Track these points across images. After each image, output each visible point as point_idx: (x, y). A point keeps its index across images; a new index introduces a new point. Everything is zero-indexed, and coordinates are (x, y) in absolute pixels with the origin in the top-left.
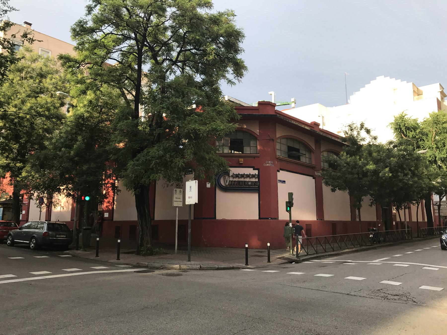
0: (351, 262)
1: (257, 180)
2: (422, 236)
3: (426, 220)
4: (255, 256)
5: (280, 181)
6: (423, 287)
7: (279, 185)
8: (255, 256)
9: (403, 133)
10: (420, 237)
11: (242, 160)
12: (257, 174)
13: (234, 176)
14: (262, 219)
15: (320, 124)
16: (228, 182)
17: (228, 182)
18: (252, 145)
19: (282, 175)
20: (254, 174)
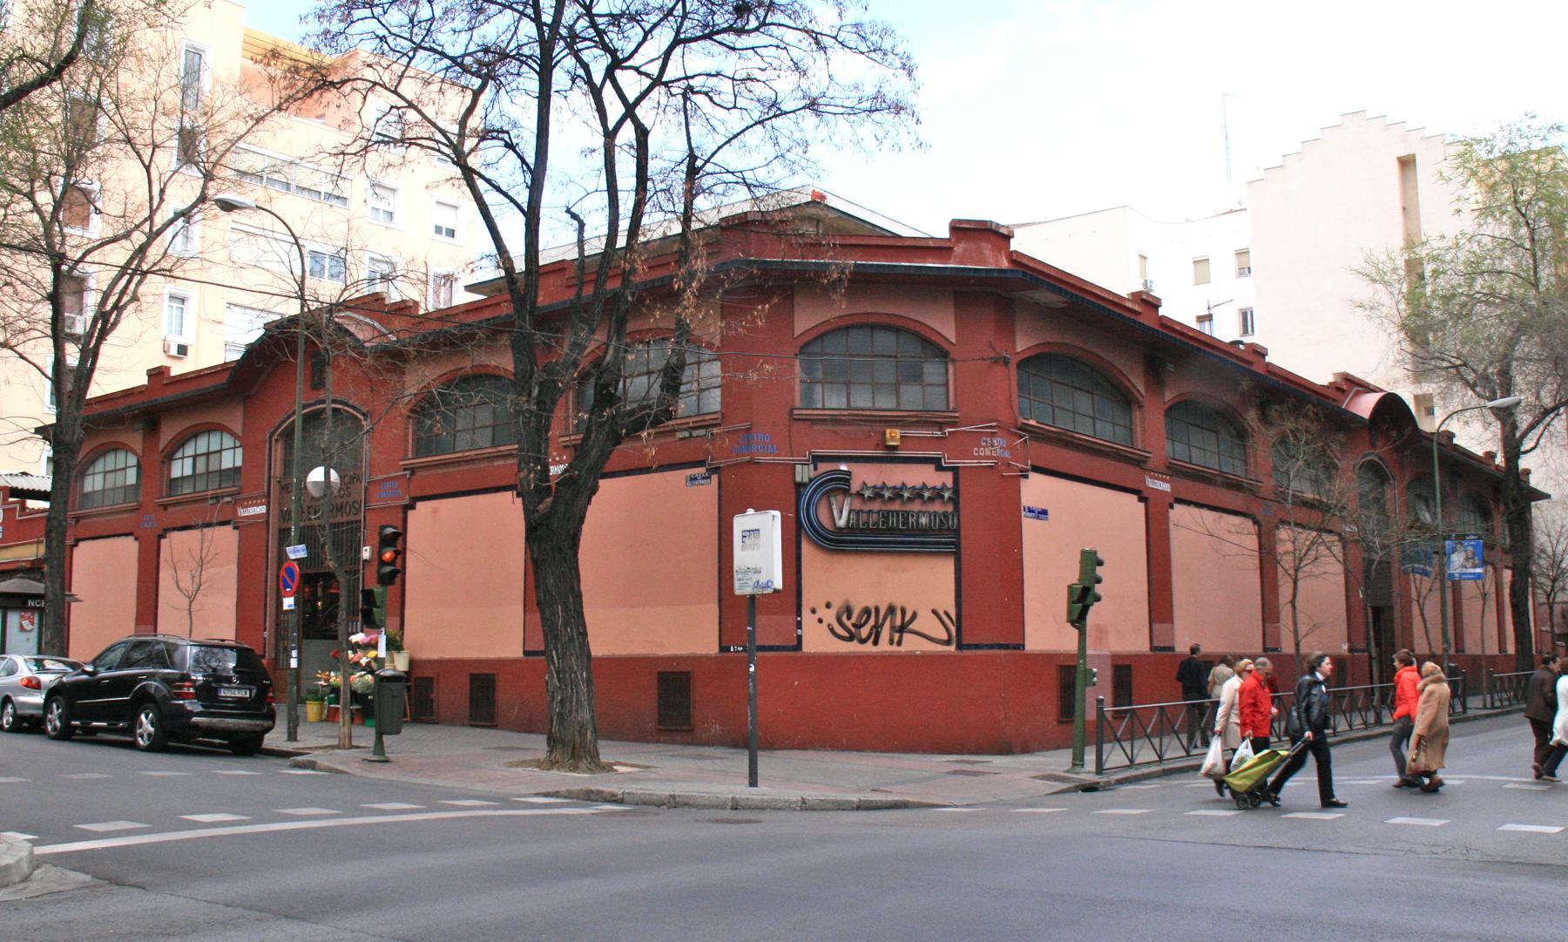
0: (1534, 523)
1: (950, 508)
2: (1498, 704)
3: (1511, 650)
4: (956, 772)
5: (1030, 511)
6: (1509, 827)
7: (1029, 525)
8: (956, 772)
9: (141, 251)
10: (1493, 707)
11: (897, 433)
12: (950, 484)
13: (867, 494)
14: (969, 647)
15: (1159, 300)
16: (845, 513)
17: (845, 513)
18: (927, 379)
19: (1036, 490)
20: (939, 485)
